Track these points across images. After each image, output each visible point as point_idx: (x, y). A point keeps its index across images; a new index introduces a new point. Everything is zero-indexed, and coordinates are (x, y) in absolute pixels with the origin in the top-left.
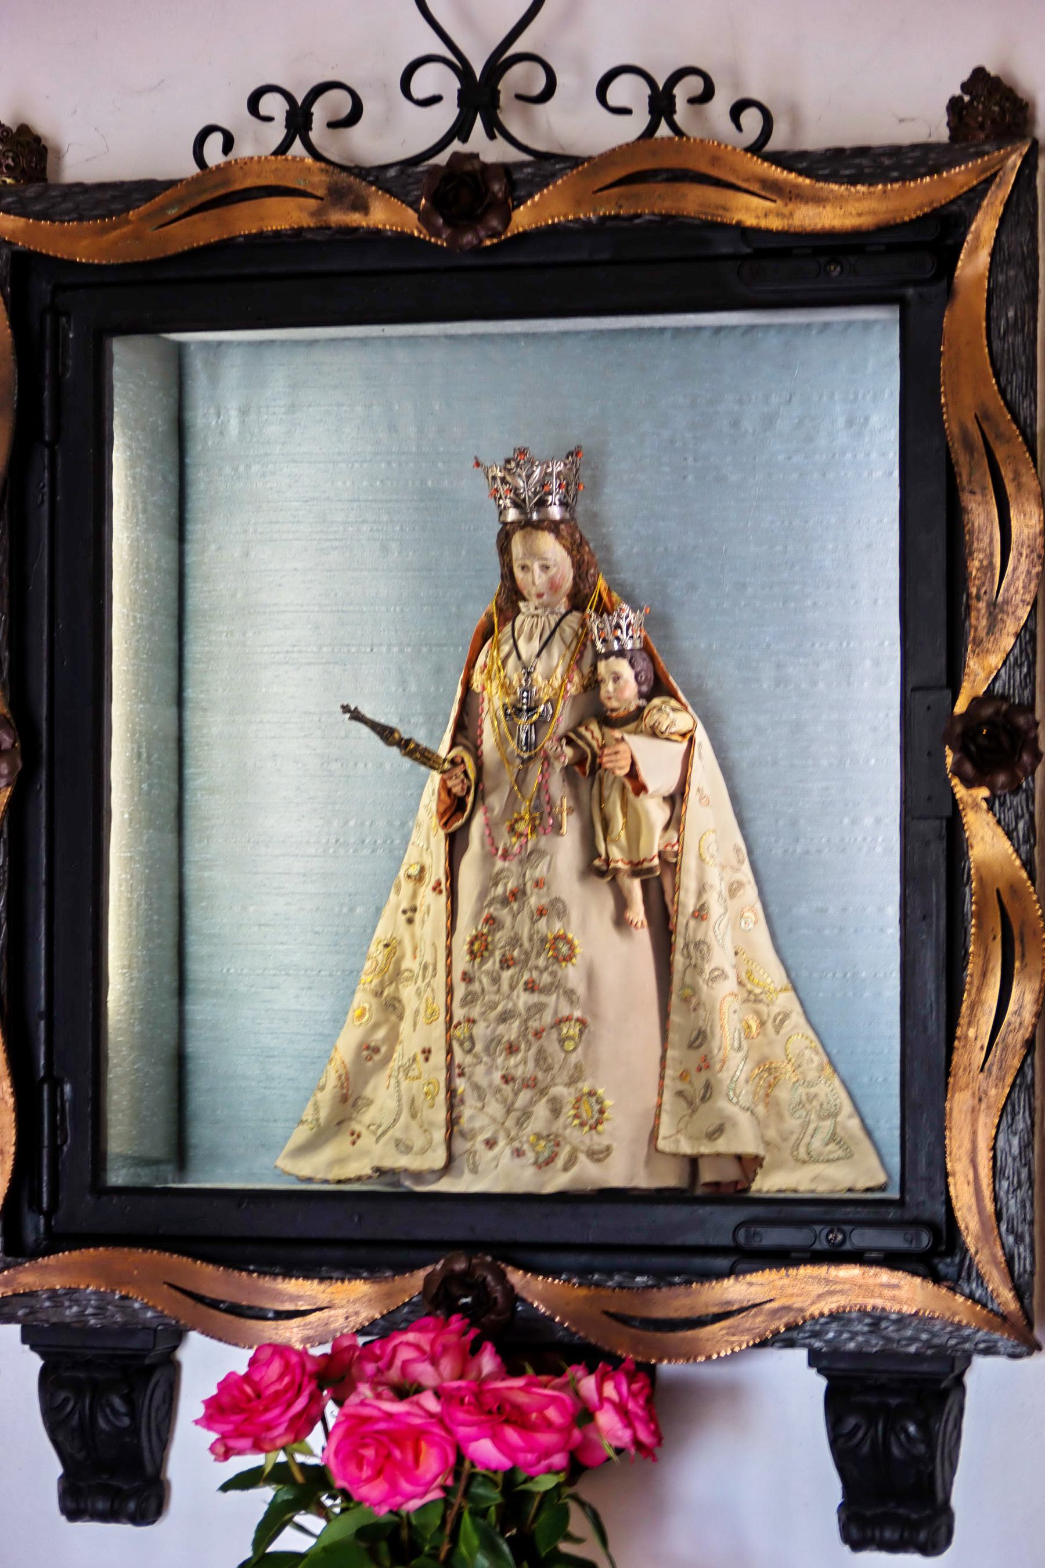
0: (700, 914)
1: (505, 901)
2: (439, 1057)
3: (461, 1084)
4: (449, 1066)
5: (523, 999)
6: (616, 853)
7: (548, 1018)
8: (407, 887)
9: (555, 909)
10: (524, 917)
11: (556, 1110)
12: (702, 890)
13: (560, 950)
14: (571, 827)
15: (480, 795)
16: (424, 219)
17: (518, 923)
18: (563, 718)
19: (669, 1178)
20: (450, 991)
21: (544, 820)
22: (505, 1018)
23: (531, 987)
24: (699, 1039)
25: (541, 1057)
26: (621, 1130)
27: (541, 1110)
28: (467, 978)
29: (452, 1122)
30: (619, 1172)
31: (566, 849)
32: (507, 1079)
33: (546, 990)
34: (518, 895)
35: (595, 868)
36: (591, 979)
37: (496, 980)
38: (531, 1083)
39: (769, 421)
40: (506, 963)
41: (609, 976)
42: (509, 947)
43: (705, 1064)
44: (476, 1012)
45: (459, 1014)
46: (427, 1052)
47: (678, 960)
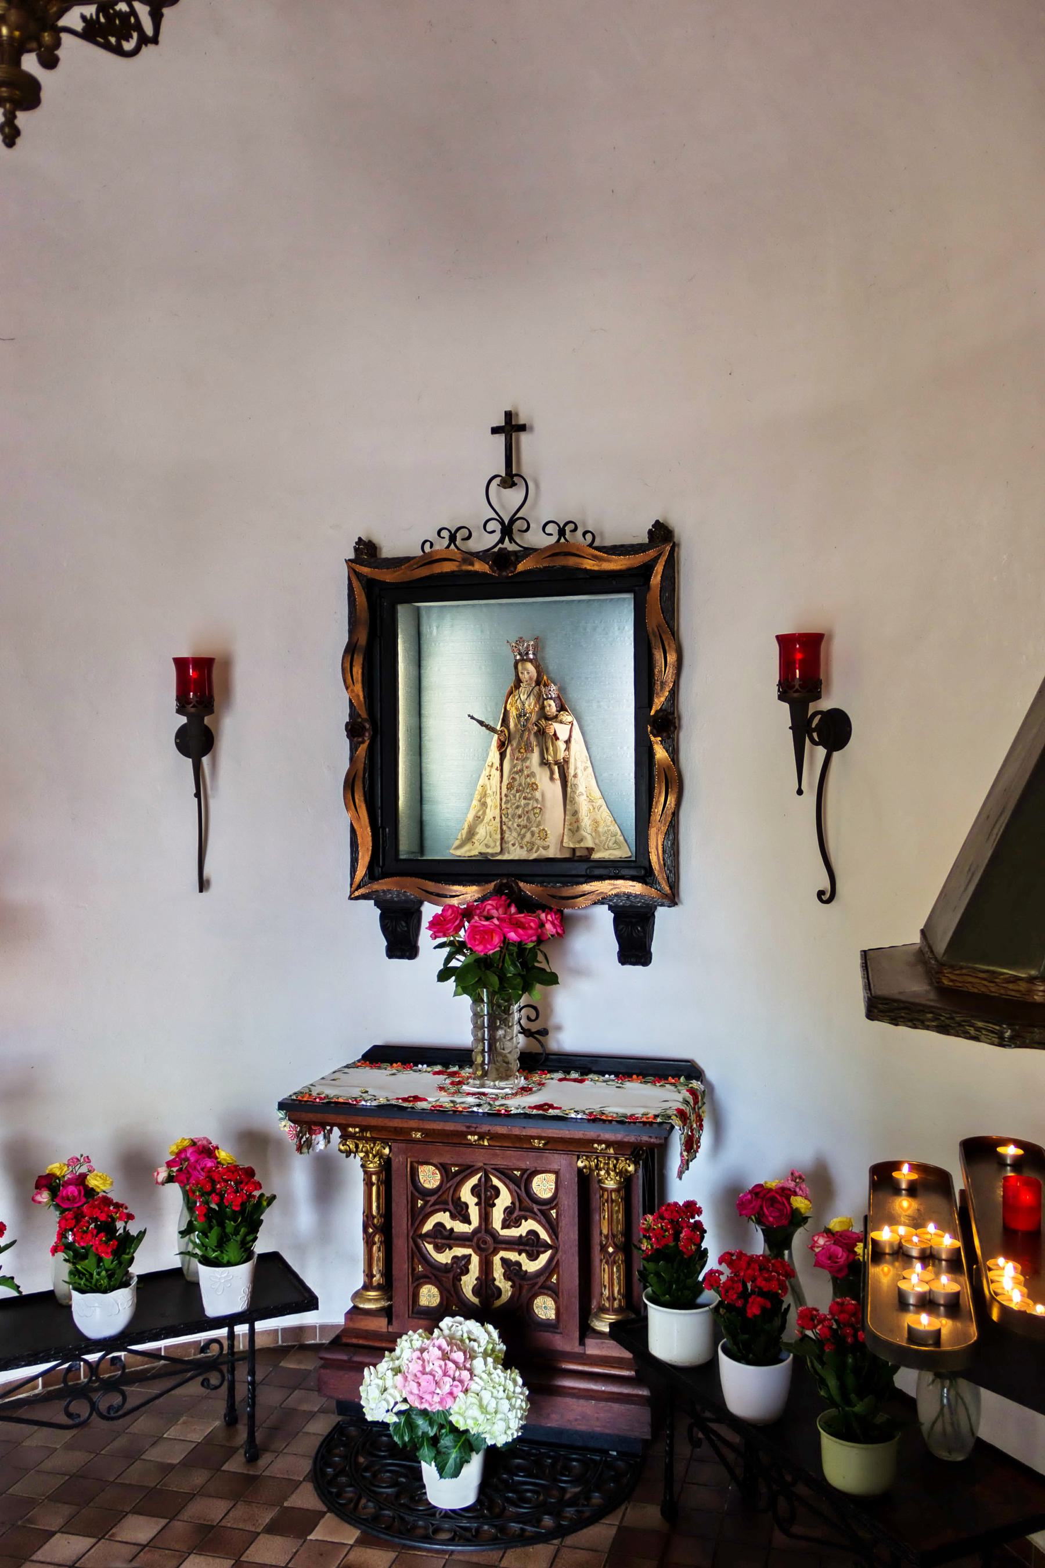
0: (575, 776)
1: (517, 773)
2: (498, 819)
3: (504, 827)
4: (501, 822)
5: (523, 802)
6: (550, 758)
7: (530, 807)
8: (488, 769)
9: (532, 775)
10: (523, 777)
11: (533, 834)
12: (576, 769)
13: (534, 787)
14: (536, 750)
15: (510, 741)
16: (490, 567)
17: (521, 779)
18: (534, 718)
19: (567, 855)
20: (501, 799)
21: (529, 748)
22: (518, 807)
23: (525, 798)
24: (575, 813)
25: (528, 819)
26: (552, 840)
27: (528, 835)
28: (506, 796)
29: (502, 839)
30: (552, 853)
31: (535, 757)
32: (518, 826)
33: (529, 799)
34: (521, 771)
35: (544, 763)
36: (543, 795)
37: (515, 796)
38: (525, 827)
39: (595, 629)
40: (517, 791)
41: (548, 796)
42: (518, 787)
43: (577, 821)
44: (509, 806)
45: (504, 806)
46: (494, 818)
47: (569, 790)
